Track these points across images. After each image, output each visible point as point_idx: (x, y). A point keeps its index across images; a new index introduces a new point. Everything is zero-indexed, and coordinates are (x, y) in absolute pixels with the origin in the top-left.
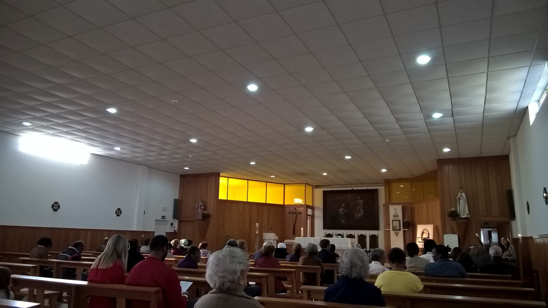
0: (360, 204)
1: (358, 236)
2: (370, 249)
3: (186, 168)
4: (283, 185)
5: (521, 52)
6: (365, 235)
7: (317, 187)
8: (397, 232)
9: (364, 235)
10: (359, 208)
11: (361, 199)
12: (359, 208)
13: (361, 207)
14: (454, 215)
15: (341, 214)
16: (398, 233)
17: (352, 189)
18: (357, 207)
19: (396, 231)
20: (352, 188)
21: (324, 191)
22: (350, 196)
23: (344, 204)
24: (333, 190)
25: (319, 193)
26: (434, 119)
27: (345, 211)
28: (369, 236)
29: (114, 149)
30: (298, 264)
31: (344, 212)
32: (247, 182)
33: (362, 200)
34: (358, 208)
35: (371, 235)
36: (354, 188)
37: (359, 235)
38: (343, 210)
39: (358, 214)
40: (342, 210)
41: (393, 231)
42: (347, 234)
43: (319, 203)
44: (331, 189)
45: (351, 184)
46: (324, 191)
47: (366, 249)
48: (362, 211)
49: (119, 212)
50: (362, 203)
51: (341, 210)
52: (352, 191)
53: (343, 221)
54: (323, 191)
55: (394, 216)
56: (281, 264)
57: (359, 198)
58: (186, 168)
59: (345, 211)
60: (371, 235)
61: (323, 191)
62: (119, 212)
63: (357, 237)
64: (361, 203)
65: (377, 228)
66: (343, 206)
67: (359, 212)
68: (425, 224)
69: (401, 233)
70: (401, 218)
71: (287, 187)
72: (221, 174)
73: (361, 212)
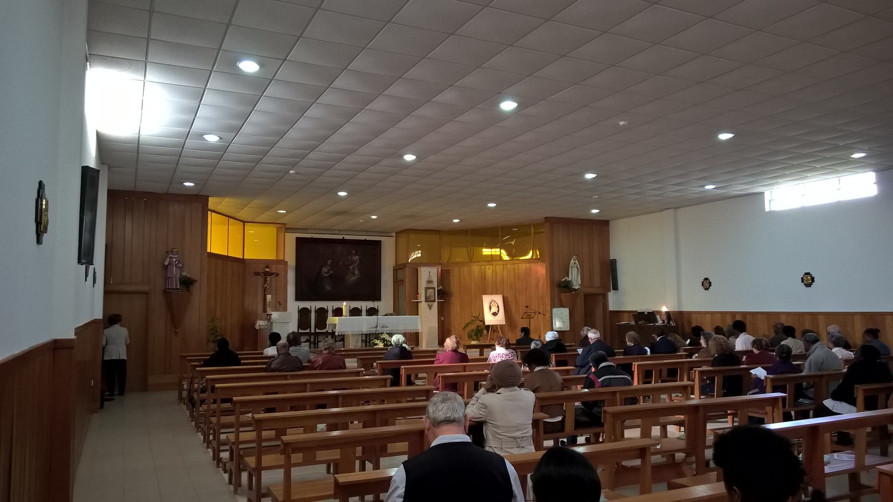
0: (353, 262)
1: (350, 310)
2: (298, 331)
3: (187, 184)
4: (242, 223)
5: (169, 65)
6: (309, 308)
7: (288, 230)
8: (431, 303)
9: (324, 308)
10: (354, 268)
11: (356, 254)
12: (354, 268)
13: (356, 267)
14: (566, 286)
15: (326, 277)
16: (432, 305)
17: (343, 237)
18: (351, 265)
19: (429, 303)
20: (343, 236)
21: (297, 238)
22: (340, 248)
23: (330, 261)
24: (365, 240)
25: (290, 240)
26: (207, 141)
27: (331, 272)
28: (333, 310)
29: (204, 139)
30: (433, 362)
31: (329, 274)
32: (227, 220)
33: (359, 256)
34: (351, 267)
35: (301, 309)
36: (347, 237)
37: (351, 309)
38: (329, 270)
39: (352, 277)
40: (326, 270)
41: (426, 303)
42: (299, 308)
43: (290, 257)
44: (363, 238)
45: (340, 231)
46: (297, 238)
47: (310, 330)
48: (356, 272)
49: (808, 280)
50: (358, 260)
51: (325, 270)
52: (343, 241)
53: (328, 288)
54: (297, 238)
55: (427, 281)
56: (239, 356)
57: (353, 252)
58: (187, 184)
59: (331, 272)
60: (300, 308)
61: (297, 238)
62: (808, 280)
63: (365, 311)
64: (356, 260)
65: (378, 298)
66: (329, 263)
67: (353, 274)
68: (492, 294)
69: (435, 305)
70: (435, 285)
71: (250, 230)
72: (212, 202)
73: (356, 272)
